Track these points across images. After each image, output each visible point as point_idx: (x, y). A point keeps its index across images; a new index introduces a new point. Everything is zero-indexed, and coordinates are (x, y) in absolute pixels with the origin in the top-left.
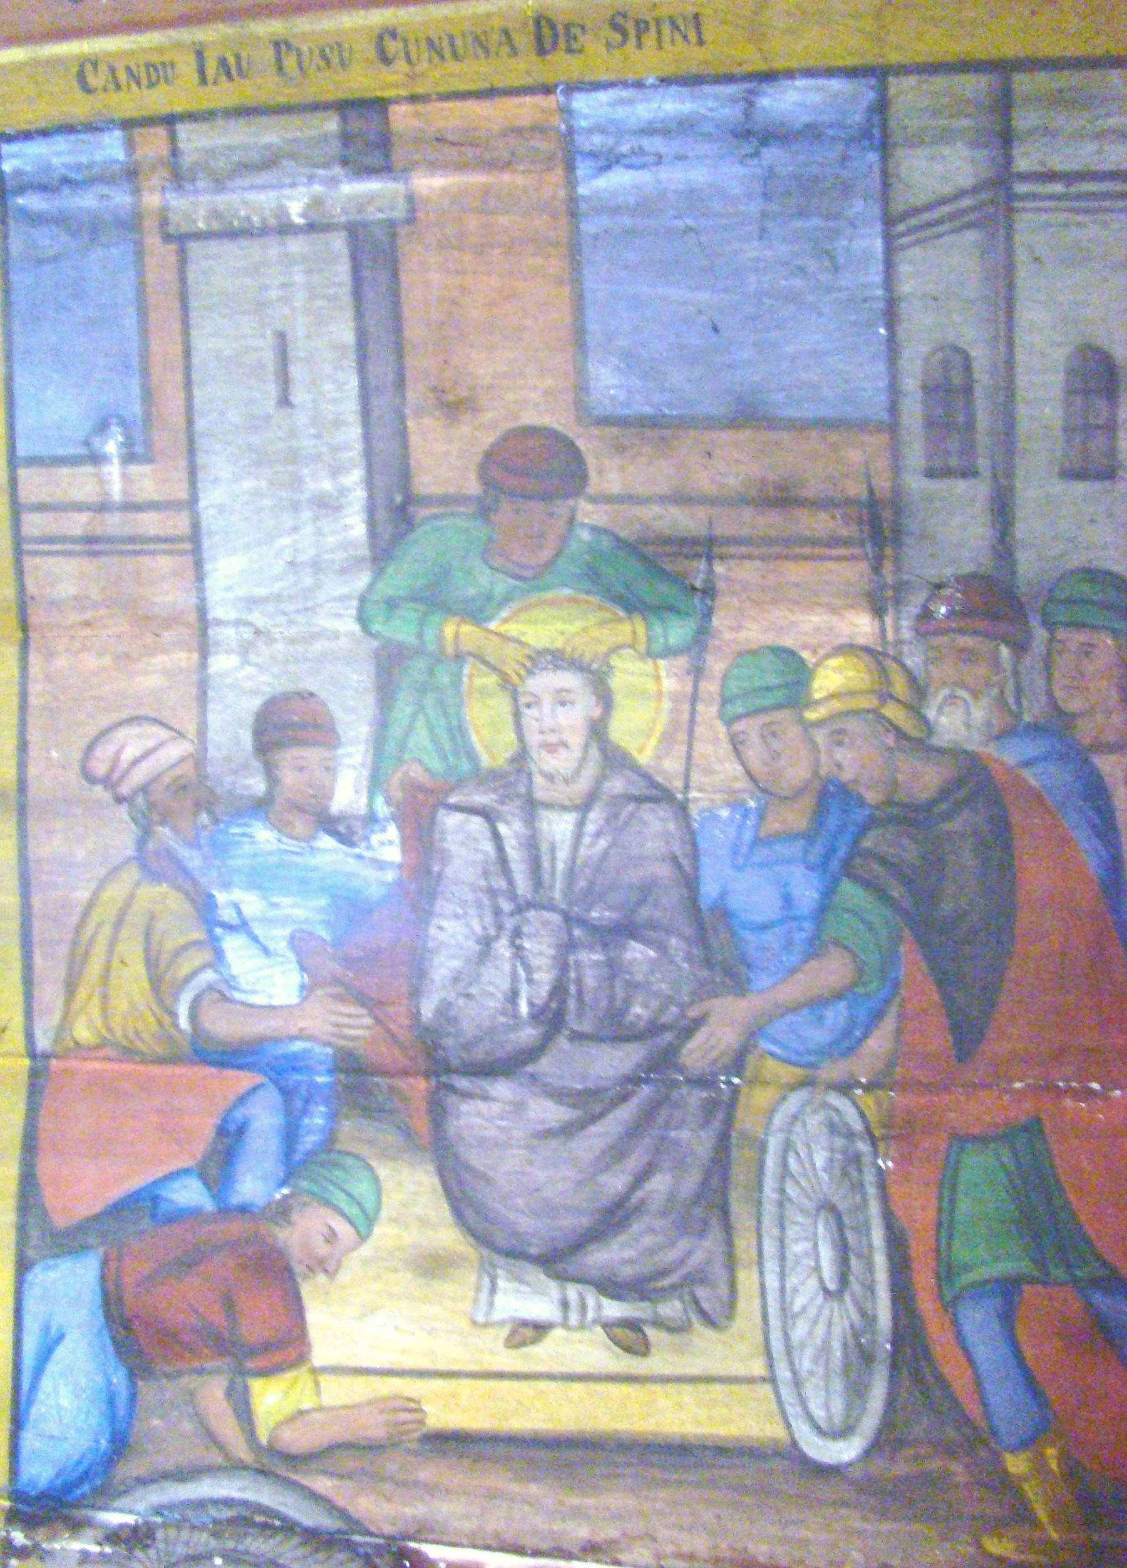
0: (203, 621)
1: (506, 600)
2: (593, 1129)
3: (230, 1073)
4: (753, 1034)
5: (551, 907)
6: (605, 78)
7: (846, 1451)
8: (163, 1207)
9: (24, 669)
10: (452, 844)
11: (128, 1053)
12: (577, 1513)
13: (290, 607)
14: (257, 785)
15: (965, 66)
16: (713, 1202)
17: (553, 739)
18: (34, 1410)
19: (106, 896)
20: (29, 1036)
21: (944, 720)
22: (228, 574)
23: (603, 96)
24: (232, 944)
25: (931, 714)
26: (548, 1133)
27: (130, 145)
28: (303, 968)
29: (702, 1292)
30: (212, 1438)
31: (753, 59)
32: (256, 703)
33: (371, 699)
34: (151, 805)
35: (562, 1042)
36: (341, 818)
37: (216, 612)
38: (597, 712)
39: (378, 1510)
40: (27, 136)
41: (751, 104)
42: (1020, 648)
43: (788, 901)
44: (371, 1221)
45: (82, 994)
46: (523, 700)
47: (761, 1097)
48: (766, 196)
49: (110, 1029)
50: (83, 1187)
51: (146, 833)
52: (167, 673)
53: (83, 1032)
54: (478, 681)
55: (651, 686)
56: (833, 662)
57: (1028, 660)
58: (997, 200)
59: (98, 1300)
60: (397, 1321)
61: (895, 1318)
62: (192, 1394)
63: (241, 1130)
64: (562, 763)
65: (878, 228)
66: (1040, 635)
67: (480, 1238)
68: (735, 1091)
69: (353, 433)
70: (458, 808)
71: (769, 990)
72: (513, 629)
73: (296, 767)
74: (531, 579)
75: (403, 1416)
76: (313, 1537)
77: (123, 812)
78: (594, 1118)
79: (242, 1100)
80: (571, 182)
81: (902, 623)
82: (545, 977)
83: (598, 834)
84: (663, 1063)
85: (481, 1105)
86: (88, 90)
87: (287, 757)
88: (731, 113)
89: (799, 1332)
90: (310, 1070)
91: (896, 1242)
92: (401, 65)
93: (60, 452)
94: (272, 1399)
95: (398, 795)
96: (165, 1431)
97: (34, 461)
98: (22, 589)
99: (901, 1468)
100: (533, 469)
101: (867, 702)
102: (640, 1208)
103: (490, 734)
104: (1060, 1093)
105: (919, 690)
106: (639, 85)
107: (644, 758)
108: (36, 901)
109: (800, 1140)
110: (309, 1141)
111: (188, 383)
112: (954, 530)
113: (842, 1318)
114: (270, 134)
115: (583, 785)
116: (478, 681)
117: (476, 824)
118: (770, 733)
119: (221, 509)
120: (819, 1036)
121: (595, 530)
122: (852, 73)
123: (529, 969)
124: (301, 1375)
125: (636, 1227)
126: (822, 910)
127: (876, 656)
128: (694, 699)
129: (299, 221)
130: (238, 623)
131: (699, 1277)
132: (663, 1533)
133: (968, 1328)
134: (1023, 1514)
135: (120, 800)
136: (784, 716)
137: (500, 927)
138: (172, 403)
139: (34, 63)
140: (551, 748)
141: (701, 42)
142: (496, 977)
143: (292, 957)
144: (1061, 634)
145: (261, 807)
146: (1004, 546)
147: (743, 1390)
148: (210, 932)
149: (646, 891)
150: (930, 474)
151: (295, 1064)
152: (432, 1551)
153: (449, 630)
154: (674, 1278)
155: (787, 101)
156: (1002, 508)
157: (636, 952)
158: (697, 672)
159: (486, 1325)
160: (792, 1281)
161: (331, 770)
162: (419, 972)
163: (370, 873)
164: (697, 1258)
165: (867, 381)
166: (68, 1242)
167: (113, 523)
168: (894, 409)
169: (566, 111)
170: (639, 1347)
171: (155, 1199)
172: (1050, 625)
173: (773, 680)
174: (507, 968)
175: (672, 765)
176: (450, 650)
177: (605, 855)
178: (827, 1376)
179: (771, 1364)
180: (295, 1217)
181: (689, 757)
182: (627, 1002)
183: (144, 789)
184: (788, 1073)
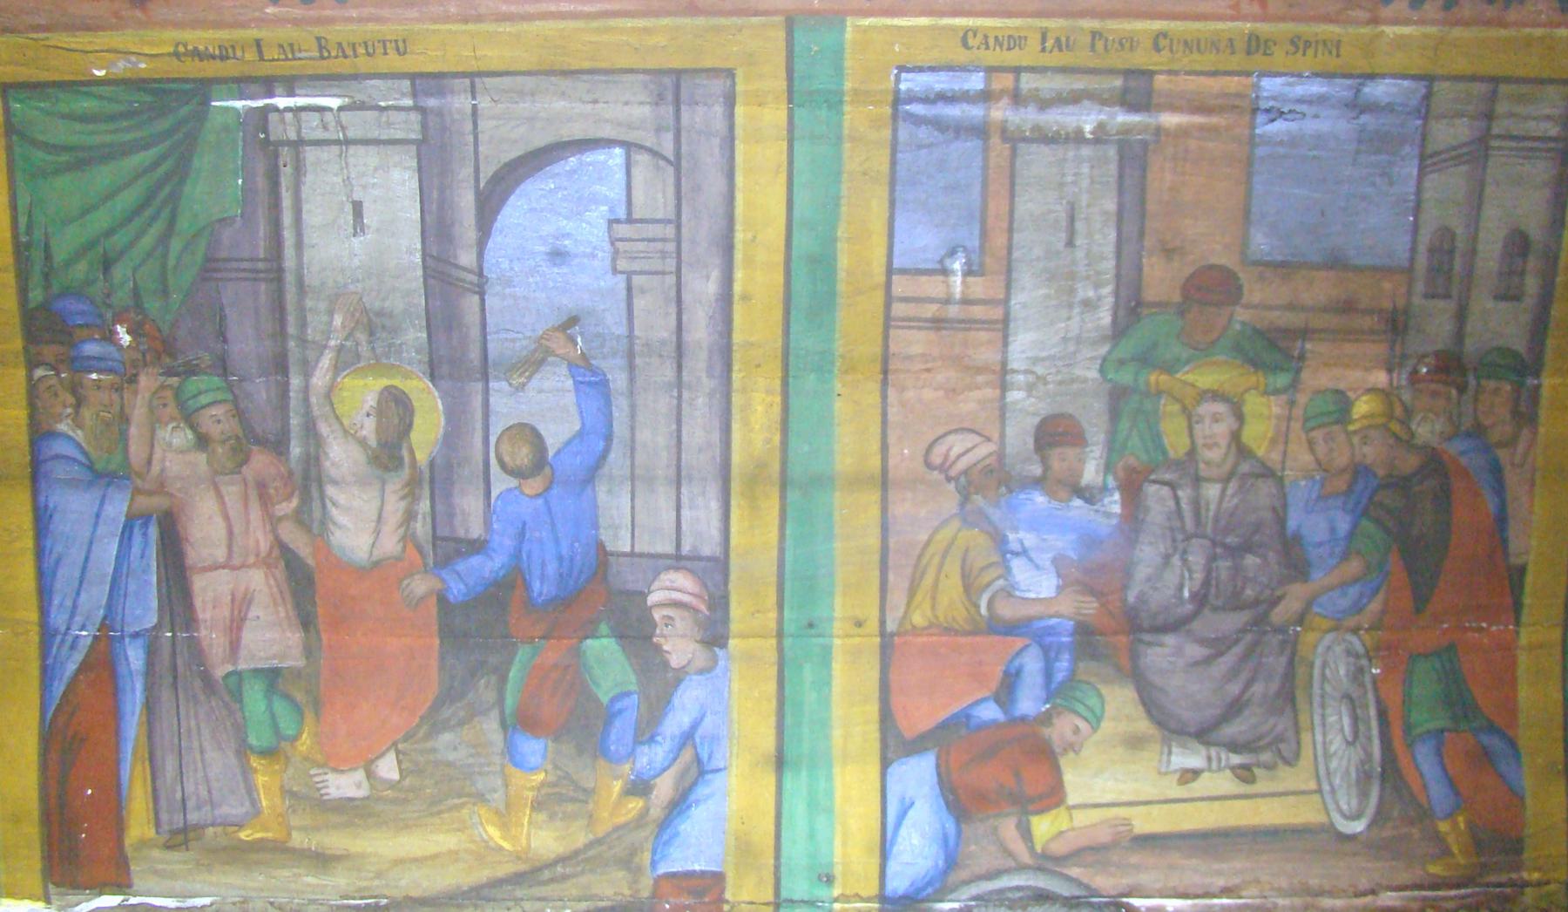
0: (1004, 369)
1: (1188, 362)
2: (1221, 660)
3: (1009, 638)
4: (1309, 604)
5: (1204, 536)
6: (1282, 70)
7: (1358, 827)
8: (973, 722)
9: (884, 397)
10: (1151, 503)
11: (949, 631)
12: (1219, 873)
13: (1060, 363)
14: (1037, 470)
15: (1474, 78)
16: (1288, 697)
17: (1209, 441)
18: (895, 849)
19: (939, 537)
20: (883, 623)
21: (1420, 430)
22: (1023, 344)
23: (1279, 80)
24: (1017, 564)
25: (1414, 427)
26: (1196, 664)
27: (987, 81)
28: (1059, 576)
29: (1282, 746)
30: (1009, 853)
31: (1362, 65)
32: (1037, 420)
33: (1106, 418)
34: (970, 483)
35: (1206, 611)
36: (1088, 487)
37: (1013, 365)
38: (1235, 426)
39: (1105, 882)
40: (920, 70)
41: (1358, 91)
42: (1462, 389)
43: (1333, 530)
44: (1099, 720)
45: (919, 597)
46: (1195, 419)
47: (1310, 637)
48: (1360, 142)
49: (936, 617)
50: (921, 715)
51: (965, 499)
52: (979, 402)
53: (918, 619)
54: (1169, 408)
55: (1266, 412)
56: (1364, 398)
57: (1465, 397)
58: (1478, 151)
59: (935, 779)
60: (1115, 779)
61: (1383, 754)
62: (996, 829)
63: (1018, 672)
64: (1215, 455)
65: (1416, 162)
66: (1472, 382)
67: (1160, 724)
68: (1297, 634)
69: (1110, 264)
70: (1155, 482)
71: (1319, 578)
72: (1190, 378)
73: (1061, 459)
74: (1202, 351)
75: (1122, 829)
76: (1069, 902)
77: (951, 486)
78: (1221, 654)
79: (1018, 654)
80: (1253, 127)
81: (1402, 378)
82: (1199, 576)
83: (1233, 496)
84: (1260, 621)
85: (1158, 649)
86: (965, 45)
87: (1055, 454)
88: (1347, 95)
89: (1334, 764)
90: (1059, 634)
91: (1382, 714)
92: (1166, 53)
93: (922, 266)
94: (1044, 827)
95: (1121, 474)
96: (981, 855)
97: (904, 272)
98: (886, 346)
99: (1388, 833)
100: (1211, 288)
101: (1381, 420)
102: (1247, 704)
103: (1175, 439)
104: (1466, 629)
105: (1408, 412)
106: (1300, 76)
107: (1260, 453)
108: (892, 542)
109: (1332, 659)
110: (1059, 677)
111: (1010, 230)
112: (1437, 326)
113: (1356, 754)
114: (1079, 83)
115: (1227, 467)
116: (1169, 408)
117: (1165, 491)
118: (1329, 438)
119: (1024, 306)
120: (1345, 603)
121: (1243, 323)
122: (1414, 77)
123: (1190, 571)
124: (1062, 810)
125: (1246, 713)
126: (1351, 535)
127: (1386, 394)
128: (1289, 419)
129: (1089, 136)
130: (1026, 372)
131: (1280, 739)
132: (1264, 878)
133: (1419, 757)
134: (1446, 852)
135: (949, 479)
136: (1335, 428)
137: (1175, 549)
138: (1000, 241)
139: (932, 28)
140: (1209, 447)
141: (1338, 56)
142: (1171, 578)
143: (1052, 569)
144: (1483, 382)
145: (1038, 483)
146: (1459, 335)
147: (1302, 798)
148: (1004, 556)
149: (1258, 527)
150: (1426, 296)
151: (1050, 631)
152: (1136, 902)
153: (1153, 378)
154: (1267, 740)
155: (1379, 90)
156: (1461, 316)
157: (1251, 560)
158: (1292, 403)
159: (1166, 774)
160: (1329, 737)
161: (1082, 461)
162: (1127, 573)
163: (1105, 521)
164: (1280, 727)
165: (1401, 245)
166: (913, 747)
167: (953, 311)
168: (1412, 260)
169: (1256, 87)
170: (1250, 780)
171: (968, 717)
172: (1477, 378)
173: (1332, 408)
174: (1178, 572)
175: (1275, 456)
176: (1153, 390)
177: (1236, 507)
178: (1349, 787)
179: (1319, 783)
180: (1055, 721)
181: (1285, 453)
182: (1243, 588)
183: (965, 472)
184: (1326, 624)
